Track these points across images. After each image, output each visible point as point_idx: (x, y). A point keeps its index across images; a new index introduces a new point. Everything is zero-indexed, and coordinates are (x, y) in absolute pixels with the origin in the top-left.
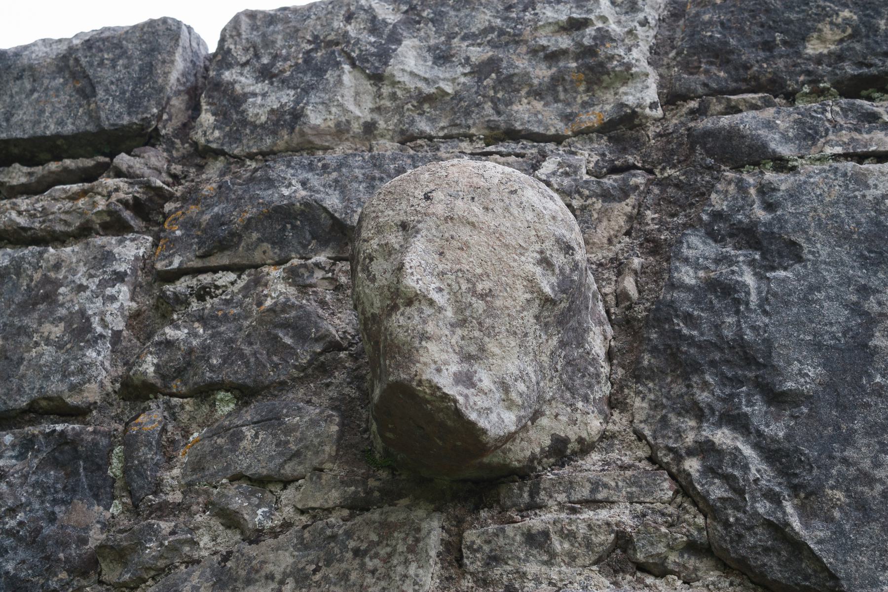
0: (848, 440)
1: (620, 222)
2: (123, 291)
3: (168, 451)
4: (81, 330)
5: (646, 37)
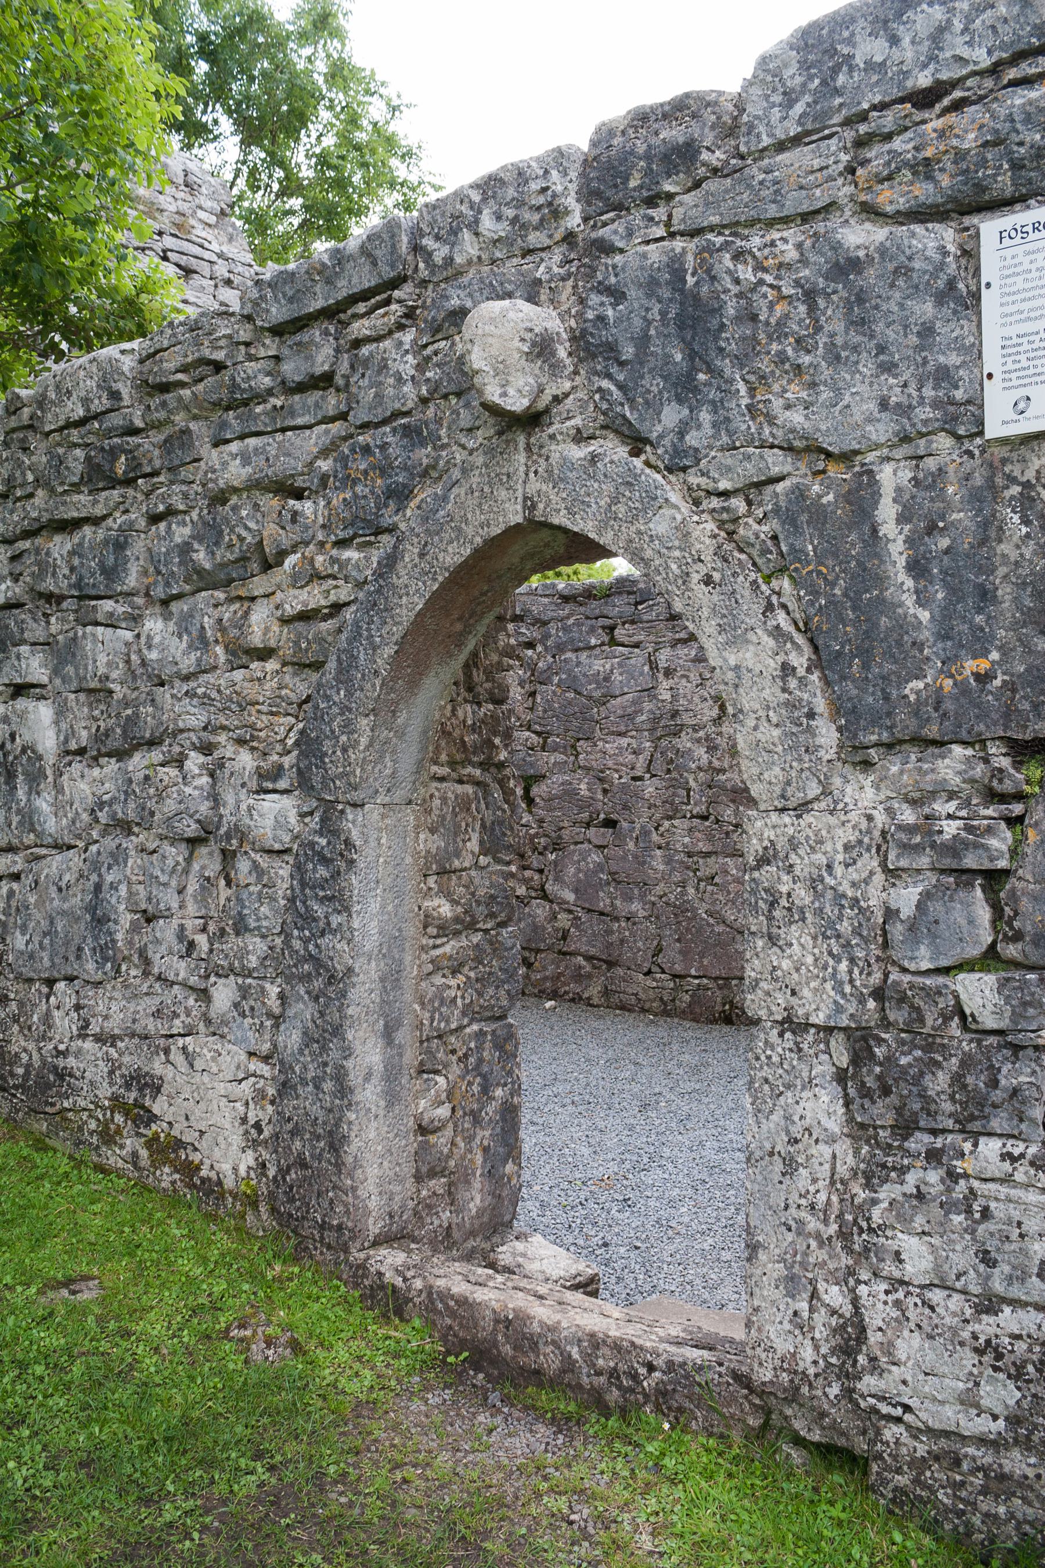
0: (642, 377)
1: (570, 290)
2: (409, 357)
3: (439, 421)
4: (400, 380)
5: (573, 187)
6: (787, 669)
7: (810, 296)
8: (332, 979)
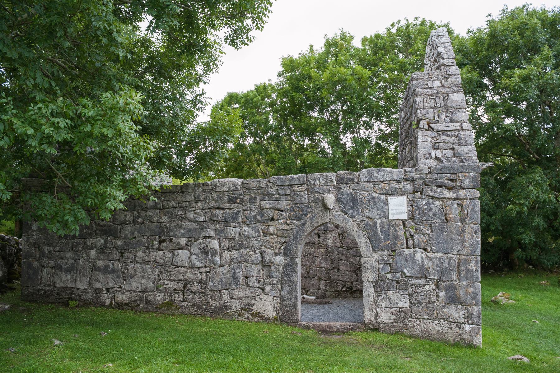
4: (305, 198)
6: (366, 242)
7: (369, 200)
8: (294, 283)
